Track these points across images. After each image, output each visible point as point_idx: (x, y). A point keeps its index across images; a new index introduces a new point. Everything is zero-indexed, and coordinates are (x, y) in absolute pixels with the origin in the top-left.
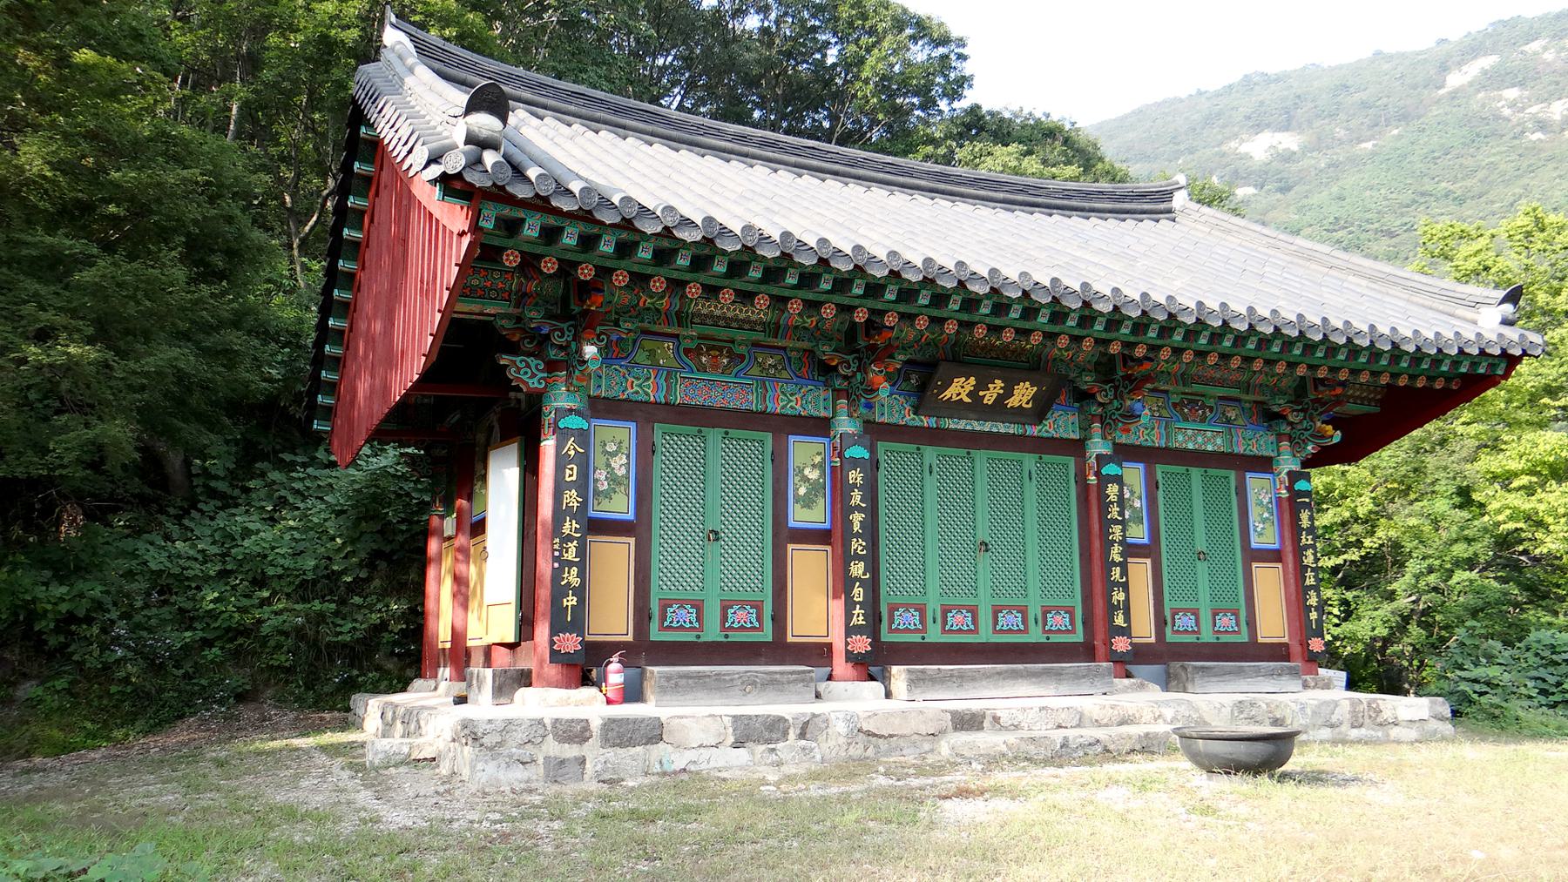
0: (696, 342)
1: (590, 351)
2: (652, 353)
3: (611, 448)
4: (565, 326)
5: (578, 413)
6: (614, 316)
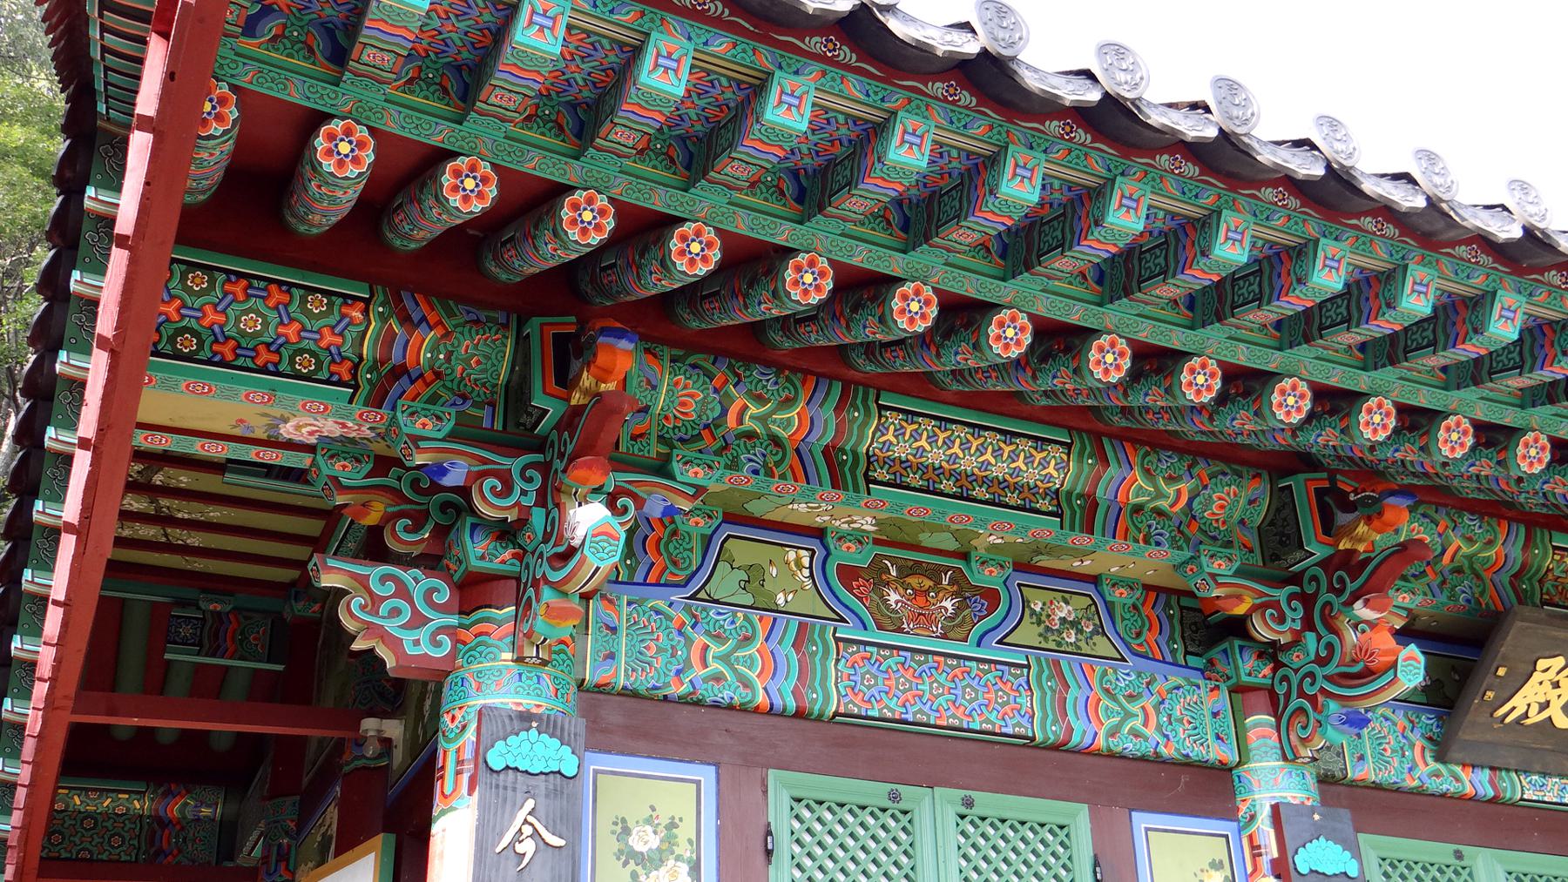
0: (871, 551)
1: (587, 518)
2: (754, 577)
3: (644, 840)
4: (515, 465)
5: (549, 726)
6: (654, 449)
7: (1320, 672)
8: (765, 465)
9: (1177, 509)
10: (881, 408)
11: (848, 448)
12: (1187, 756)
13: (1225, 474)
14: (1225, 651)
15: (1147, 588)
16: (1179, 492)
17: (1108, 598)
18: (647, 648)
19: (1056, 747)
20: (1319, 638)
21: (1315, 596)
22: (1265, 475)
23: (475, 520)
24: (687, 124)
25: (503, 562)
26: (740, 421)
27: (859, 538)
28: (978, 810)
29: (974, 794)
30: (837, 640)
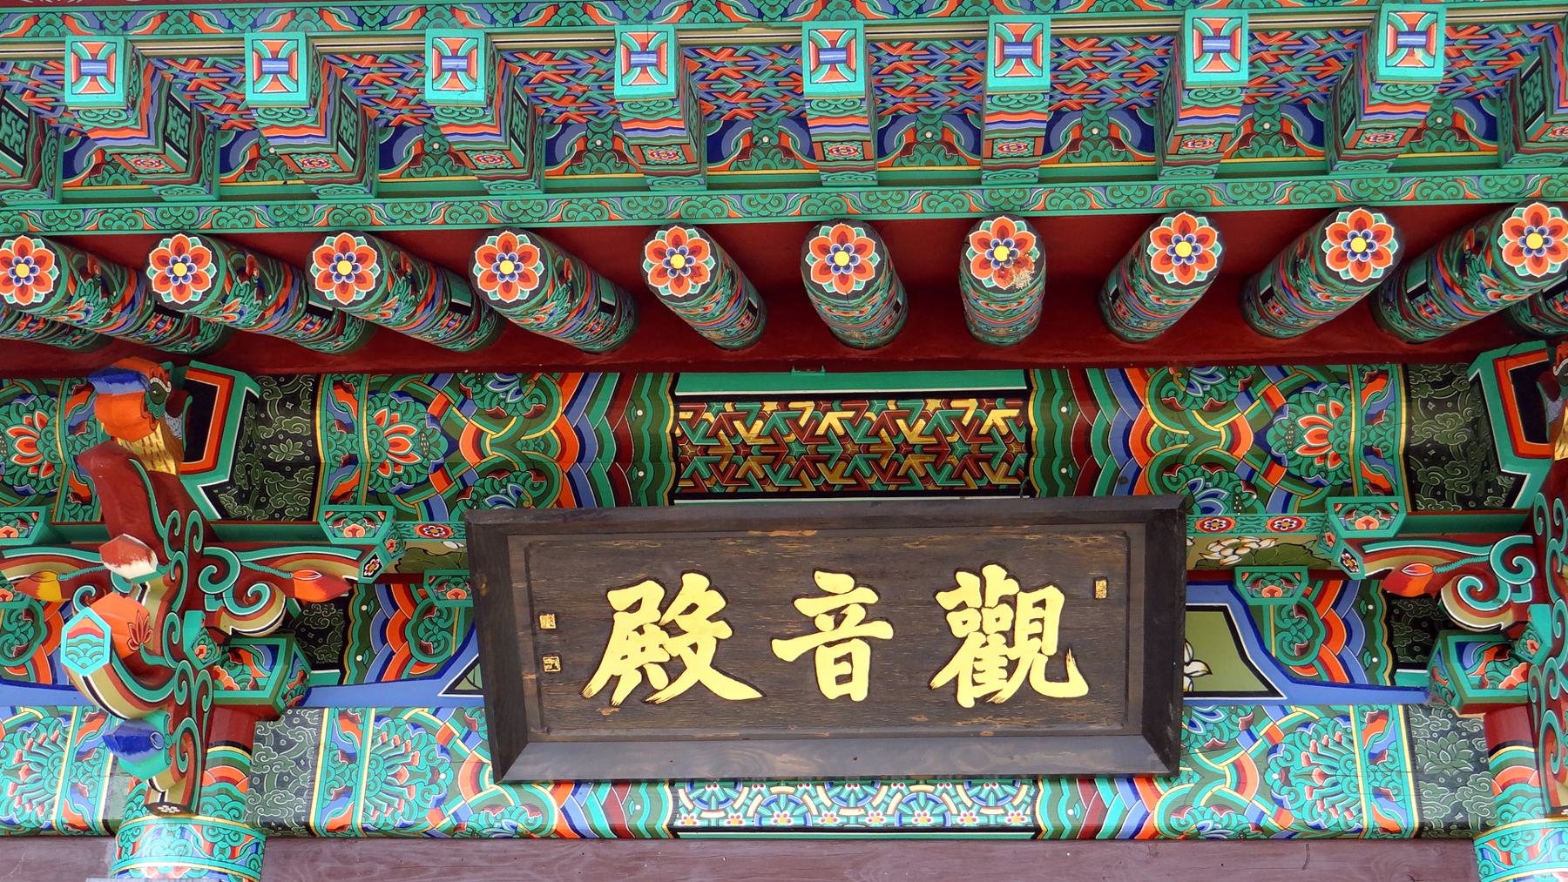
4: (1492, 554)
10: (678, 401)
13: (24, 396)
16: (1233, 427)
22: (1396, 370)
23: (1461, 638)
24: (1289, 89)
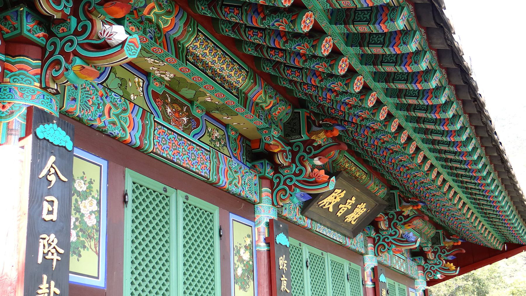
7: (294, 178)
8: (155, 37)
9: (267, 109)
11: (181, 42)
12: (247, 197)
14: (262, 163)
15: (240, 134)
17: (229, 134)
18: (89, 101)
19: (212, 184)
20: (297, 167)
21: (298, 152)
25: (38, 37)
26: (149, 13)
27: (161, 80)
28: (189, 202)
29: (189, 196)
30: (155, 121)
